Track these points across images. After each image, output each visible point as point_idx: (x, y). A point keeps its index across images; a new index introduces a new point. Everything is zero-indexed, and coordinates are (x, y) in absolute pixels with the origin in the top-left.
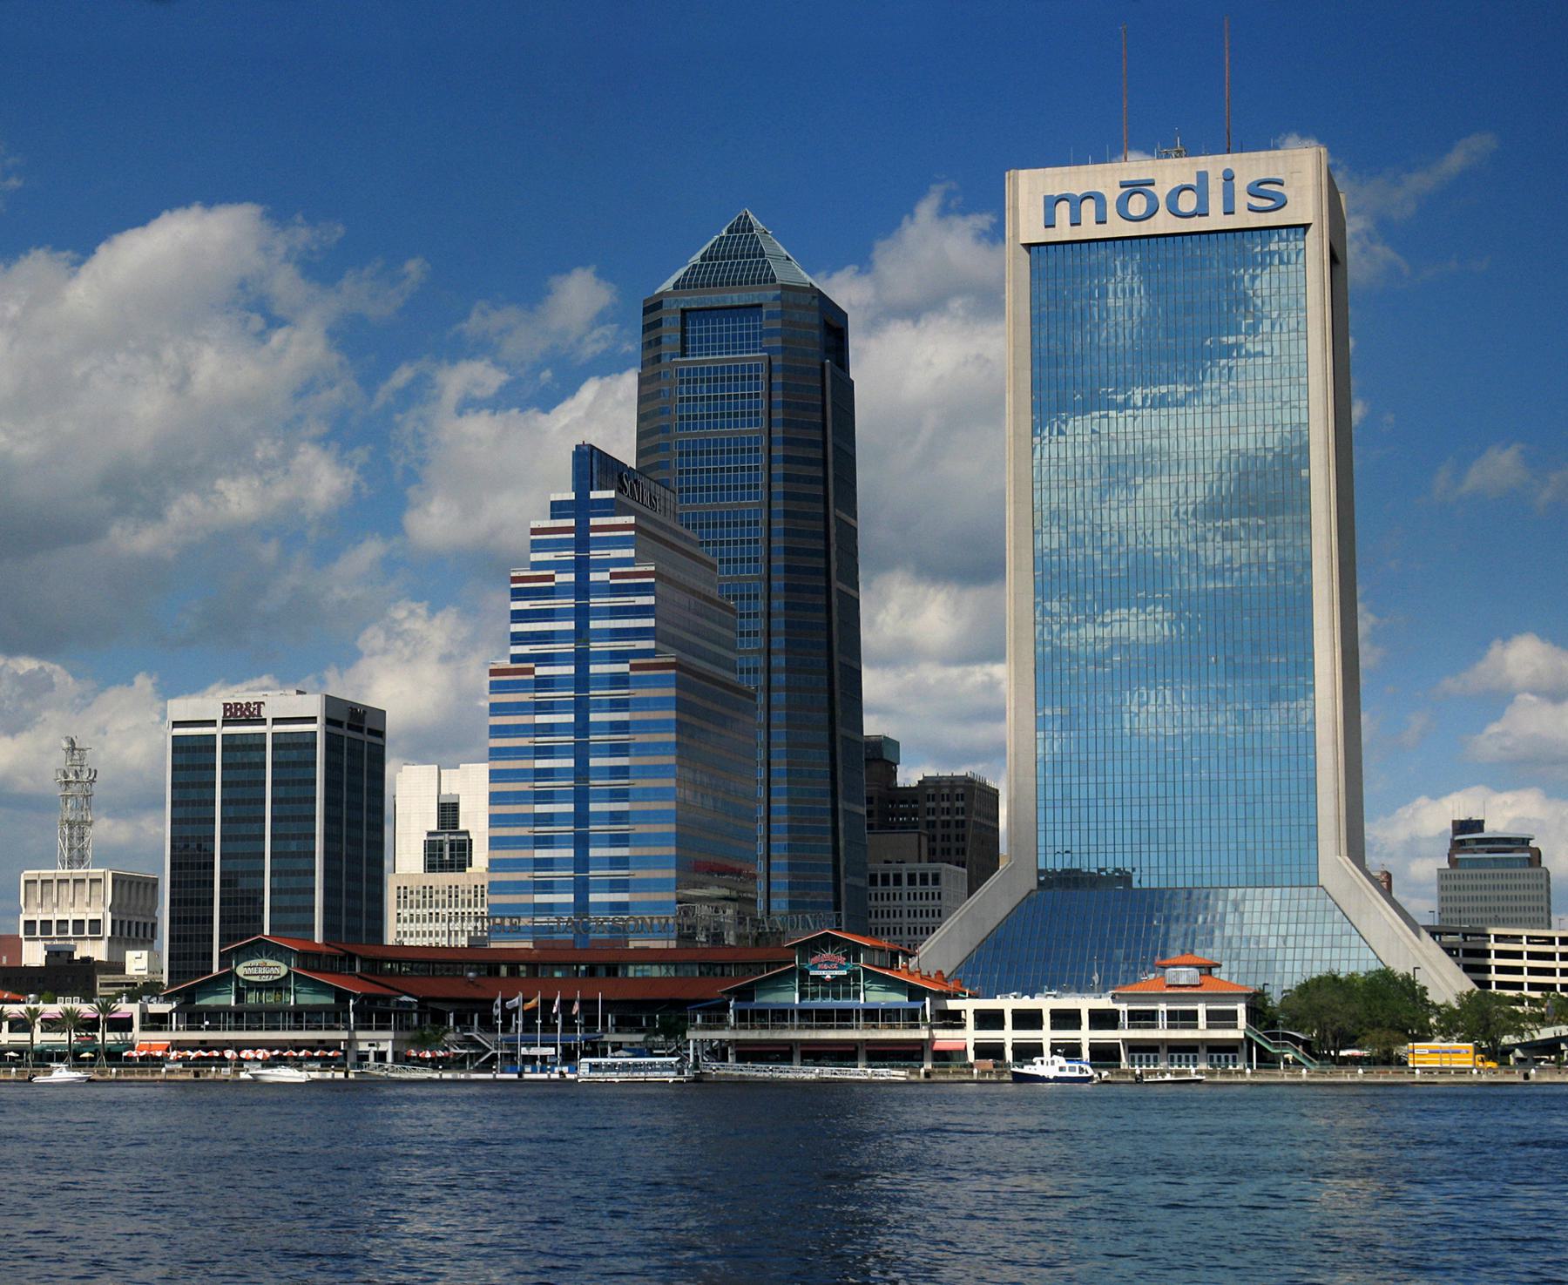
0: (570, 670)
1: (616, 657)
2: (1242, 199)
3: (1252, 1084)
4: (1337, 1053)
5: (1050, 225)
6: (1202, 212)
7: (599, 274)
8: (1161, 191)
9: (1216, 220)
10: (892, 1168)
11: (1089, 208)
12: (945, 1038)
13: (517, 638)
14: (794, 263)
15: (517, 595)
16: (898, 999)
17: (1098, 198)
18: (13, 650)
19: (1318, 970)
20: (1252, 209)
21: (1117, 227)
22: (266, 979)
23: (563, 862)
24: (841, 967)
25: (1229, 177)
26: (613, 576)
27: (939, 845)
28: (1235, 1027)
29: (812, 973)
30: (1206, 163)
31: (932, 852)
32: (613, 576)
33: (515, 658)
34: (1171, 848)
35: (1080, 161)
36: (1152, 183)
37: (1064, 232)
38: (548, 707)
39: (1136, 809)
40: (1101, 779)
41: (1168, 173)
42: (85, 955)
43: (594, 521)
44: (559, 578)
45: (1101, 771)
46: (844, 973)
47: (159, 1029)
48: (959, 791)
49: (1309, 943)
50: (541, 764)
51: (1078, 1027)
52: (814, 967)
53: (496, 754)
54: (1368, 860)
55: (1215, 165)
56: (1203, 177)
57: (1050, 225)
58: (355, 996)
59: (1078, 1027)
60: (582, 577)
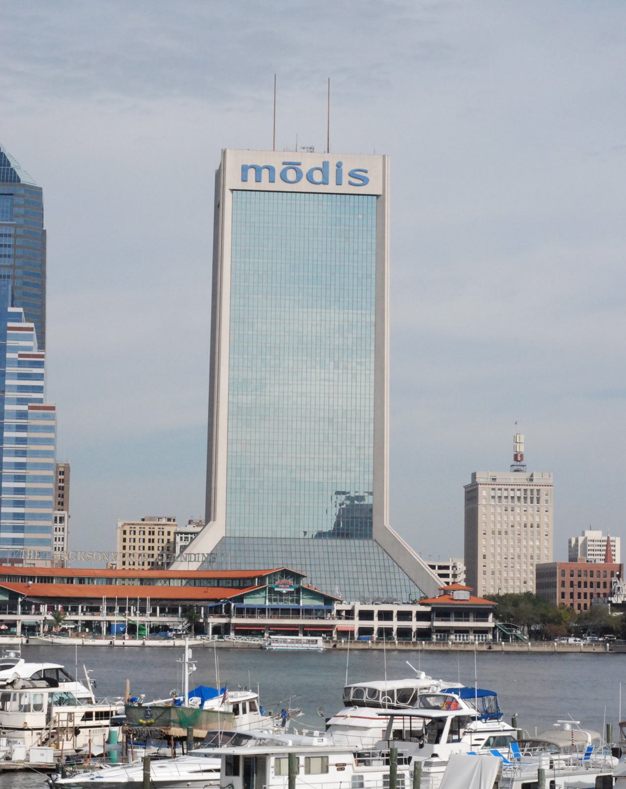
1: (21, 401)
2: (346, 178)
5: (244, 179)
11: (265, 173)
14: (425, 564)
16: (319, 603)
17: (271, 169)
18: (612, 787)
20: (350, 183)
23: (10, 428)
24: (291, 587)
26: (20, 356)
29: (276, 589)
32: (20, 356)
34: (297, 517)
36: (299, 164)
37: (251, 184)
40: (365, 264)
42: (369, 177)
46: (292, 590)
48: (62, 469)
49: (372, 556)
51: (372, 619)
52: (278, 587)
54: (168, 756)
56: (326, 164)
58: (22, 596)
59: (372, 619)
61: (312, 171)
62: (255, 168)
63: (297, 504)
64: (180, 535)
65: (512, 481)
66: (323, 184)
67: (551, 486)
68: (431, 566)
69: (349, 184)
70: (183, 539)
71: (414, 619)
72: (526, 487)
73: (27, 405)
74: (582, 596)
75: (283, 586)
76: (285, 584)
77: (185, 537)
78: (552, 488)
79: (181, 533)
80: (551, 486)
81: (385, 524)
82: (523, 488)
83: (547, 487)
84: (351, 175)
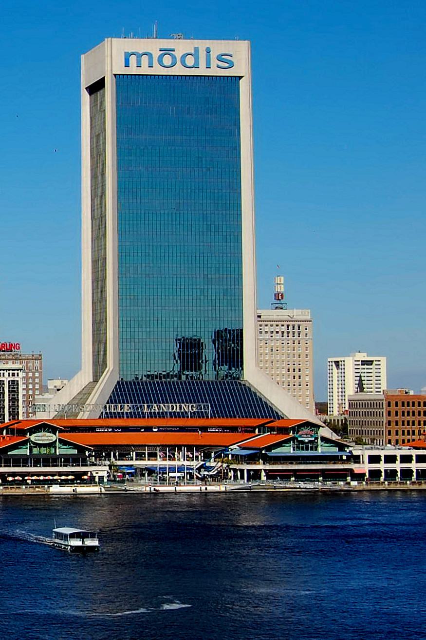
2: (214, 62)
5: (127, 65)
6: (196, 66)
7: (354, 471)
8: (178, 54)
9: (202, 71)
10: (421, 501)
11: (145, 60)
12: (356, 468)
19: (158, 56)
21: (158, 70)
22: (48, 442)
25: (208, 51)
29: (299, 439)
30: (197, 43)
39: (164, 344)
41: (182, 46)
45: (233, 305)
52: (300, 436)
55: (202, 45)
56: (197, 50)
57: (127, 65)
61: (184, 56)
64: (8, 372)
65: (275, 318)
67: (310, 321)
69: (217, 67)
70: (11, 374)
71: (414, 462)
72: (289, 323)
74: (406, 423)
75: (305, 436)
76: (306, 434)
77: (12, 373)
78: (311, 323)
79: (9, 370)
80: (310, 321)
82: (287, 323)
83: (307, 322)
84: (219, 58)
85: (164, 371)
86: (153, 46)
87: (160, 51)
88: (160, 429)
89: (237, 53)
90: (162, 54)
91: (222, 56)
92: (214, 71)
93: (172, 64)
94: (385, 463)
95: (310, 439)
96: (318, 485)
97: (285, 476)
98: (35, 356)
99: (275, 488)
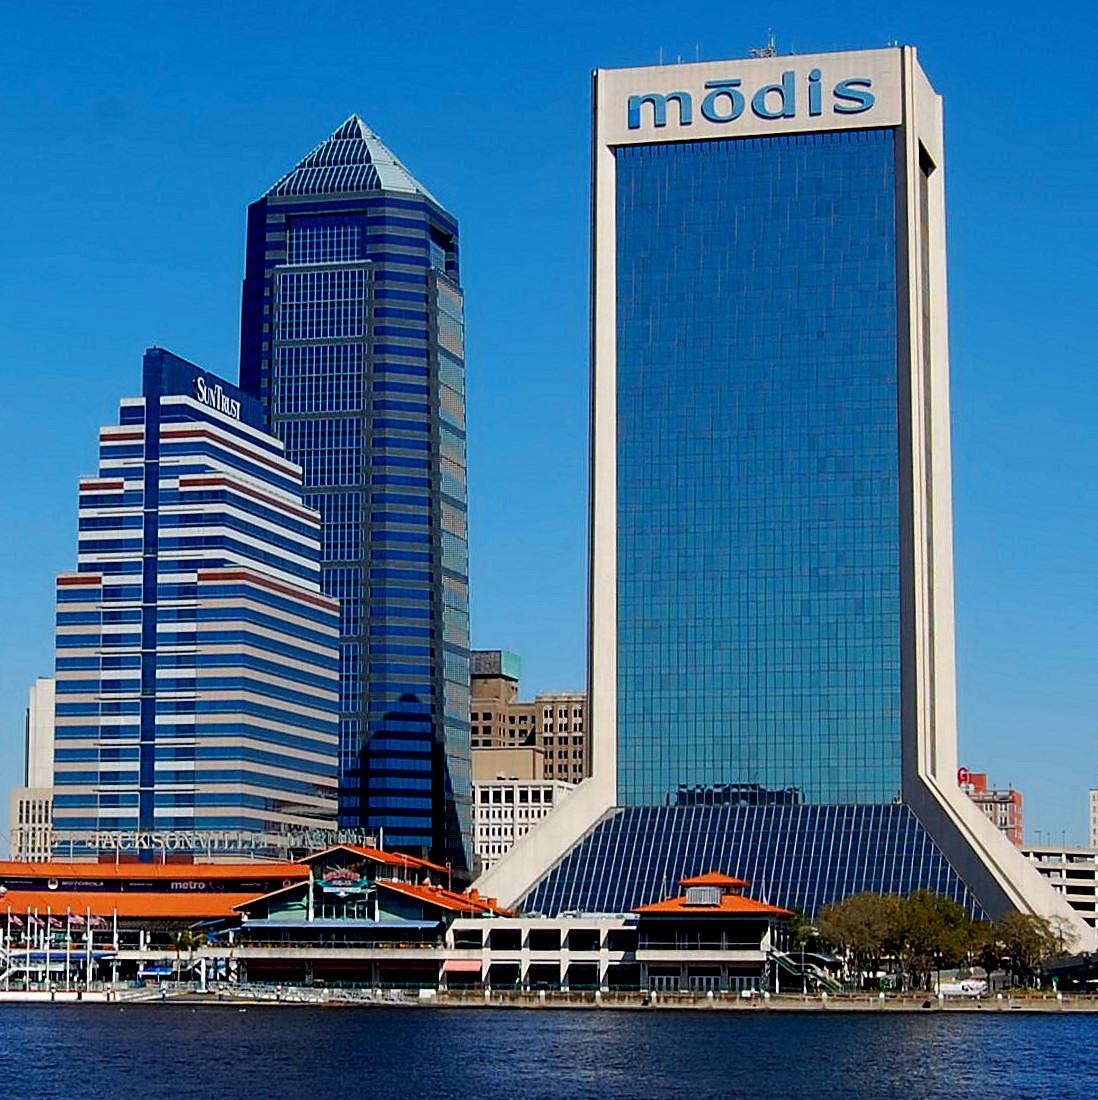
0: (161, 628)
2: (828, 101)
3: (544, 1009)
4: (874, 974)
5: (634, 125)
8: (747, 92)
9: (802, 123)
11: (673, 109)
13: (87, 547)
15: (86, 502)
24: (355, 884)
26: (183, 483)
27: (557, 762)
28: (757, 948)
29: (326, 890)
31: (549, 769)
32: (183, 483)
33: (83, 567)
35: (670, 61)
38: (178, 776)
41: (755, 74)
43: (164, 428)
44: (129, 485)
47: (130, 948)
50: (190, 627)
52: (329, 883)
53: (63, 664)
55: (800, 65)
56: (788, 78)
57: (634, 125)
60: (152, 484)
61: (761, 94)
62: (653, 101)
63: (753, 740)
66: (786, 117)
68: (1023, 853)
69: (836, 111)
73: (196, 572)
75: (340, 883)
76: (343, 879)
81: (921, 773)
85: (717, 786)
86: (691, 78)
87: (707, 87)
88: (64, 883)
89: (884, 76)
90: (713, 93)
91: (848, 85)
92: (829, 121)
93: (733, 113)
94: (519, 931)
95: (351, 890)
96: (373, 995)
97: (291, 972)
98: (998, 793)
99: (260, 1000)
